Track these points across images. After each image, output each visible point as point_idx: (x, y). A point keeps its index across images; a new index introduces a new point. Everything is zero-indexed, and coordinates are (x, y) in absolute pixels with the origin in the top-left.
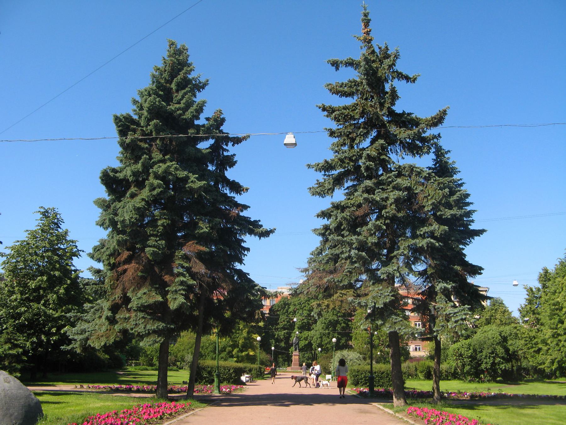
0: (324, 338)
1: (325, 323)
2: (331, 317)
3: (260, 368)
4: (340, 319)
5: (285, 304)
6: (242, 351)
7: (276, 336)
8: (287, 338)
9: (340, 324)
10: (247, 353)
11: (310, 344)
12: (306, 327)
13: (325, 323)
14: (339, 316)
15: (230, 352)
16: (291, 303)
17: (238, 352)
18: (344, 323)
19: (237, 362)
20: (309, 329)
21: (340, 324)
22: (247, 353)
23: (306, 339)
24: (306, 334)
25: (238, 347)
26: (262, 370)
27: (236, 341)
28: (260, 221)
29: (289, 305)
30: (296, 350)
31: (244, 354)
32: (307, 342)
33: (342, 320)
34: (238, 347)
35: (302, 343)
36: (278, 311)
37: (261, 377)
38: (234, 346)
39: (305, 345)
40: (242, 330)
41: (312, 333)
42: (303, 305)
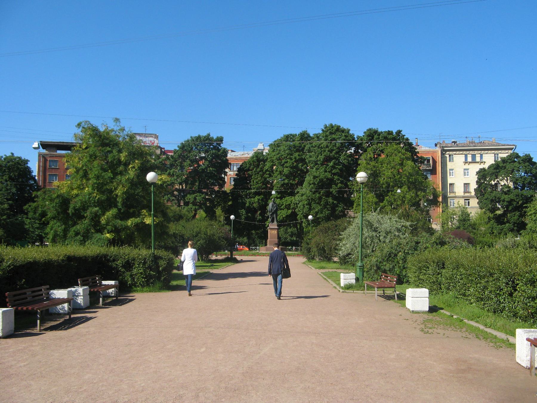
0: (313, 205)
1: (314, 184)
2: (322, 173)
3: (156, 258)
4: (336, 177)
5: (259, 160)
6: (124, 216)
7: (247, 205)
8: (263, 208)
9: (336, 185)
10: (138, 220)
11: (294, 215)
12: (288, 191)
13: (314, 184)
14: (334, 174)
15: (96, 218)
16: (267, 159)
17: (116, 217)
18: (342, 182)
19: (112, 242)
20: (292, 194)
21: (336, 185)
22: (138, 220)
23: (288, 207)
24: (288, 200)
25: (116, 206)
26: (162, 264)
27: (111, 191)
28: (304, 263)
29: (265, 161)
30: (273, 221)
31: (130, 222)
32: (290, 211)
33: (339, 180)
34: (116, 206)
35: (283, 213)
36: (249, 170)
37: (158, 285)
38: (108, 203)
39: (287, 216)
40: (126, 164)
41: (297, 198)
42: (283, 161)
